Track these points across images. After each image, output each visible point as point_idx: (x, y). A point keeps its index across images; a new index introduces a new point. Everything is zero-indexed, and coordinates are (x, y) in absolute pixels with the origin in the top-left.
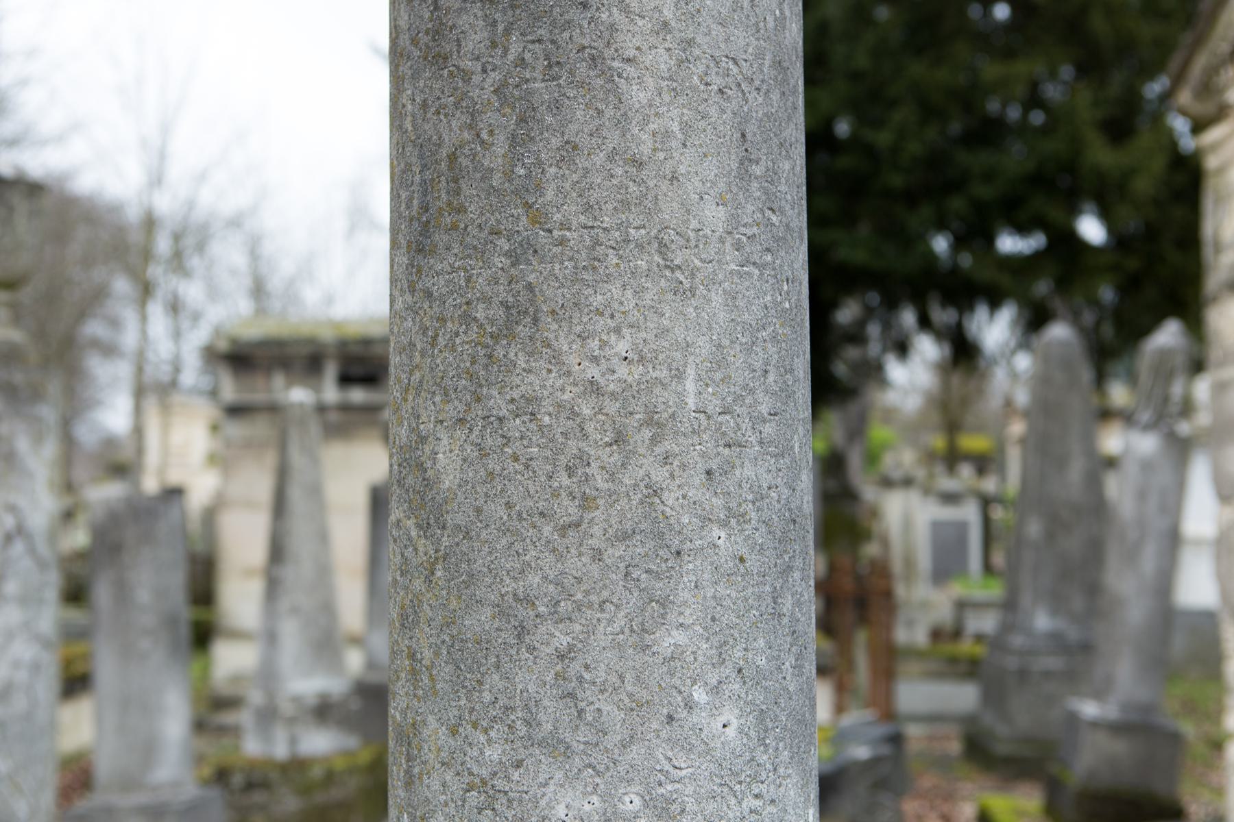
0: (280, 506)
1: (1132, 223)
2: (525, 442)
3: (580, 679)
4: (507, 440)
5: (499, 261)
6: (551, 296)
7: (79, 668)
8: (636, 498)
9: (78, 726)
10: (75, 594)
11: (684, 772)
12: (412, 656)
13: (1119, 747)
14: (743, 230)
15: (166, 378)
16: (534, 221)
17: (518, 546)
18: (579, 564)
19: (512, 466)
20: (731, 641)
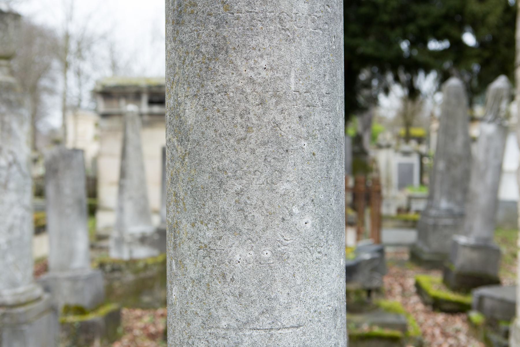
0: (124, 155)
1: (487, 37)
2: (222, 104)
3: (246, 203)
4: (215, 103)
5: (211, 27)
6: (234, 41)
7: (42, 223)
8: (270, 127)
9: (42, 247)
10: (40, 193)
11: (289, 242)
12: (176, 195)
13: (474, 255)
14: (316, 14)
15: (76, 104)
16: (226, 10)
17: (220, 148)
18: (245, 155)
19: (217, 114)
20: (309, 188)
